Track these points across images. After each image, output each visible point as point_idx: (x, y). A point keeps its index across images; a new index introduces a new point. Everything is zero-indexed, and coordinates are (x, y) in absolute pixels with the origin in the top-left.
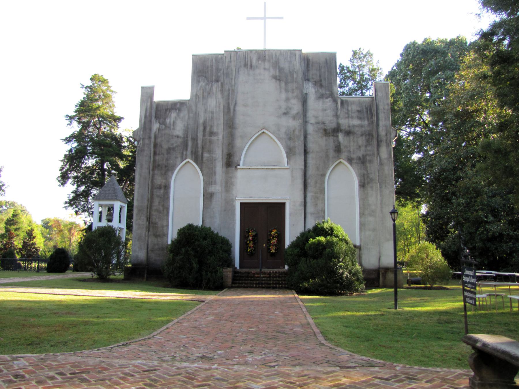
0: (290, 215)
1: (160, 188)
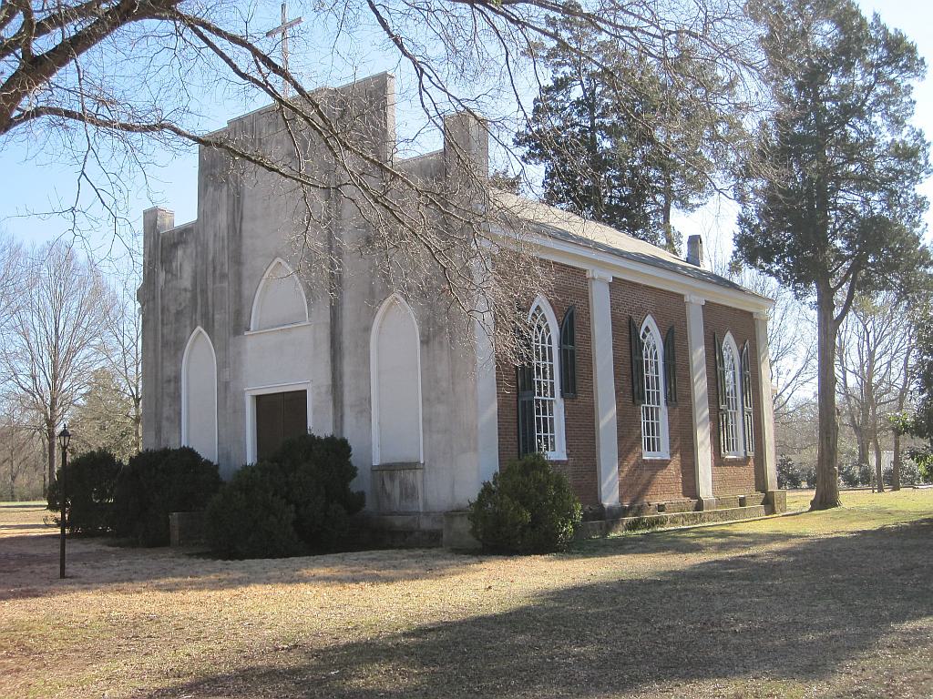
0: (314, 414)
1: (169, 381)
